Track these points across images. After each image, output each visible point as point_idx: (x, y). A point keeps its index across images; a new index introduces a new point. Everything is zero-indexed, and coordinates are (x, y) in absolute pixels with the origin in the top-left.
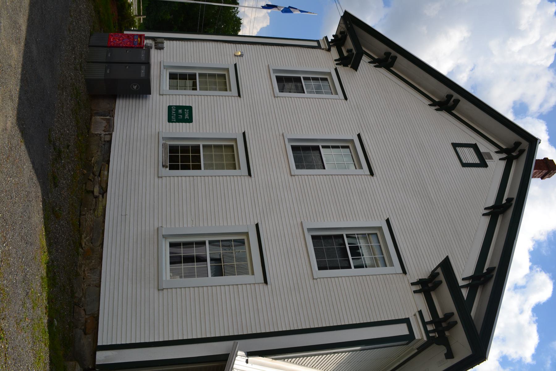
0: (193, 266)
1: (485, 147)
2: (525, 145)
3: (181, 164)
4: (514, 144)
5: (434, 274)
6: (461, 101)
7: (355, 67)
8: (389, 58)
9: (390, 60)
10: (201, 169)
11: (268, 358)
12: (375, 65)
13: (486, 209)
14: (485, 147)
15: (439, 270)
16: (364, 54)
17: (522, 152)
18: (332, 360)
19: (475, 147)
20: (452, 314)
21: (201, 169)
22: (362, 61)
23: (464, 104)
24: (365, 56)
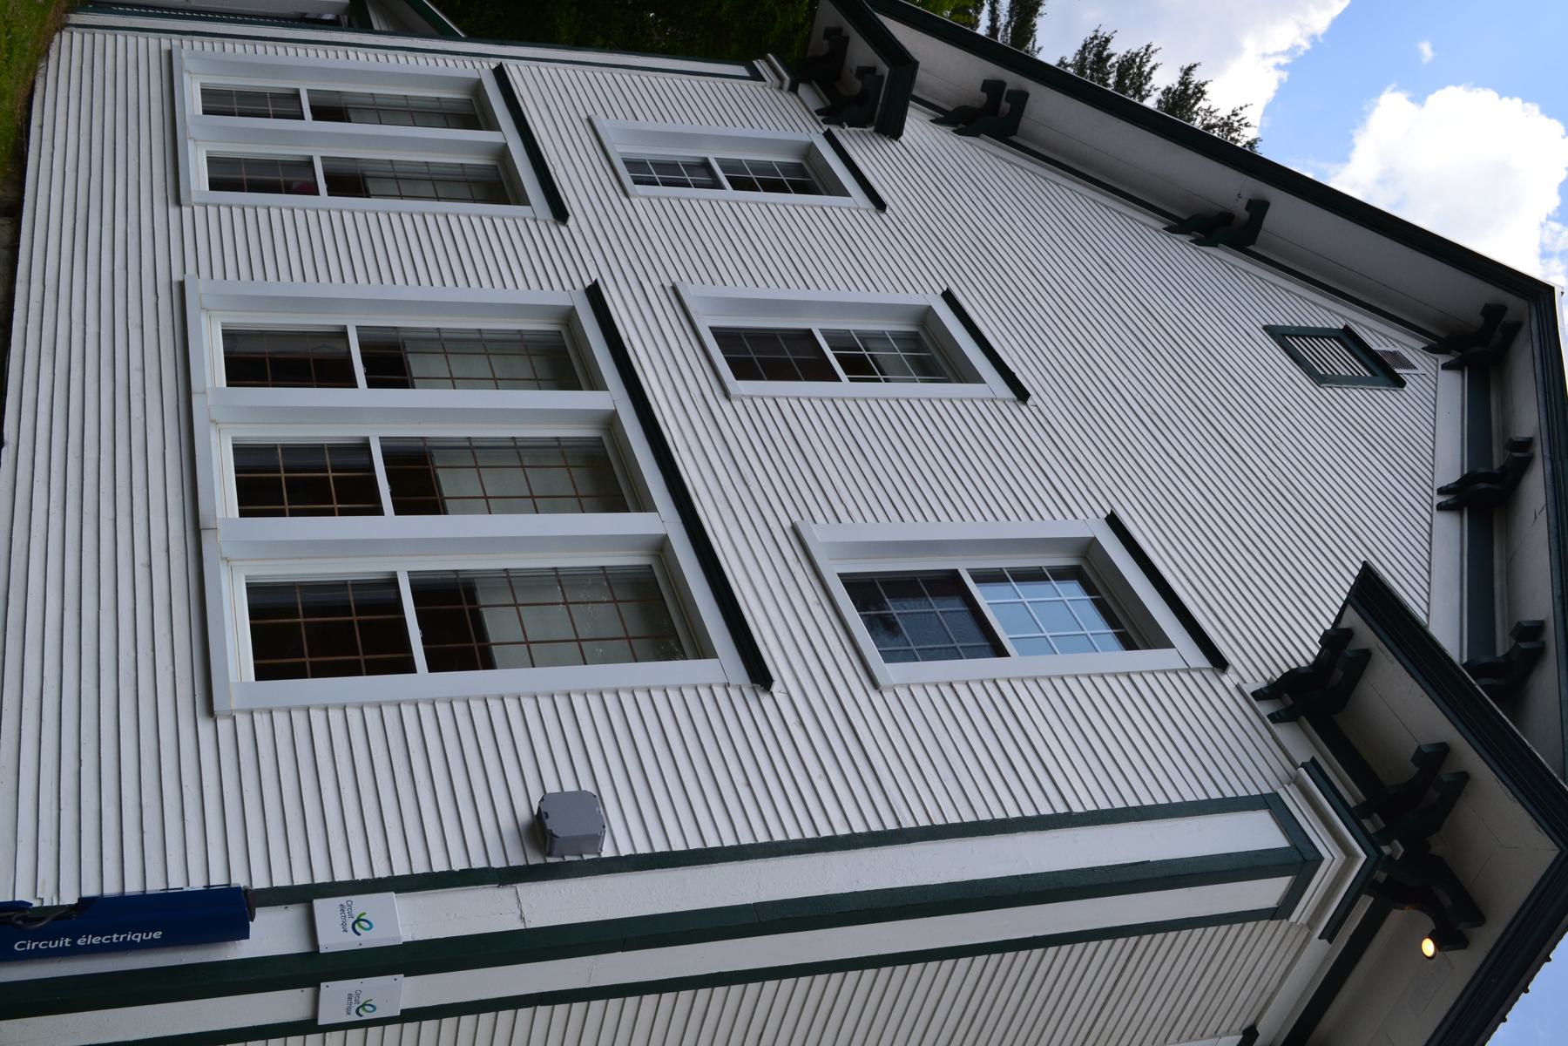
0: (353, 626)
1: (1380, 337)
2: (1515, 304)
3: (286, 478)
4: (1482, 314)
5: (1335, 640)
6: (1271, 206)
7: (892, 129)
8: (1000, 101)
9: (1005, 106)
10: (415, 672)
11: (802, 142)
12: (955, 128)
13: (1441, 491)
14: (1380, 337)
15: (1353, 619)
16: (911, 102)
17: (1513, 330)
18: (1205, 338)
19: (1347, 337)
20: (1443, 750)
21: (415, 672)
22: (907, 118)
23: (1284, 210)
24: (915, 107)
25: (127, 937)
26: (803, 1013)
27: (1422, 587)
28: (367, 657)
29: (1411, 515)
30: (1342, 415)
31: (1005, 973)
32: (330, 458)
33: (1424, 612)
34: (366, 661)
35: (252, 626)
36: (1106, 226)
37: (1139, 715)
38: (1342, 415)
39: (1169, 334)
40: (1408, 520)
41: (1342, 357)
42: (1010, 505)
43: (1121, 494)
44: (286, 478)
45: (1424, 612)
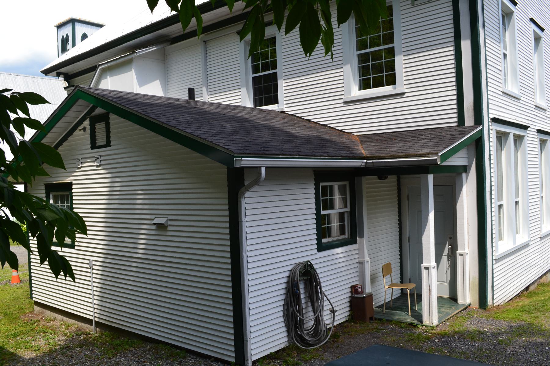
3: (370, 64)
25: (377, 40)
26: (411, 45)
27: (527, 19)
28: (371, 78)
29: (526, 27)
30: (547, 10)
31: (493, 24)
32: (257, 97)
33: (498, 27)
34: (383, 75)
35: (274, 104)
36: (546, 11)
37: (446, 39)
38: (547, 10)
39: (525, 17)
40: (526, 27)
41: (538, 13)
42: (492, 26)
43: (214, 89)
44: (370, 64)
45: (498, 27)
